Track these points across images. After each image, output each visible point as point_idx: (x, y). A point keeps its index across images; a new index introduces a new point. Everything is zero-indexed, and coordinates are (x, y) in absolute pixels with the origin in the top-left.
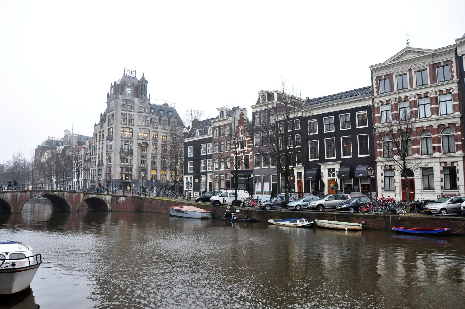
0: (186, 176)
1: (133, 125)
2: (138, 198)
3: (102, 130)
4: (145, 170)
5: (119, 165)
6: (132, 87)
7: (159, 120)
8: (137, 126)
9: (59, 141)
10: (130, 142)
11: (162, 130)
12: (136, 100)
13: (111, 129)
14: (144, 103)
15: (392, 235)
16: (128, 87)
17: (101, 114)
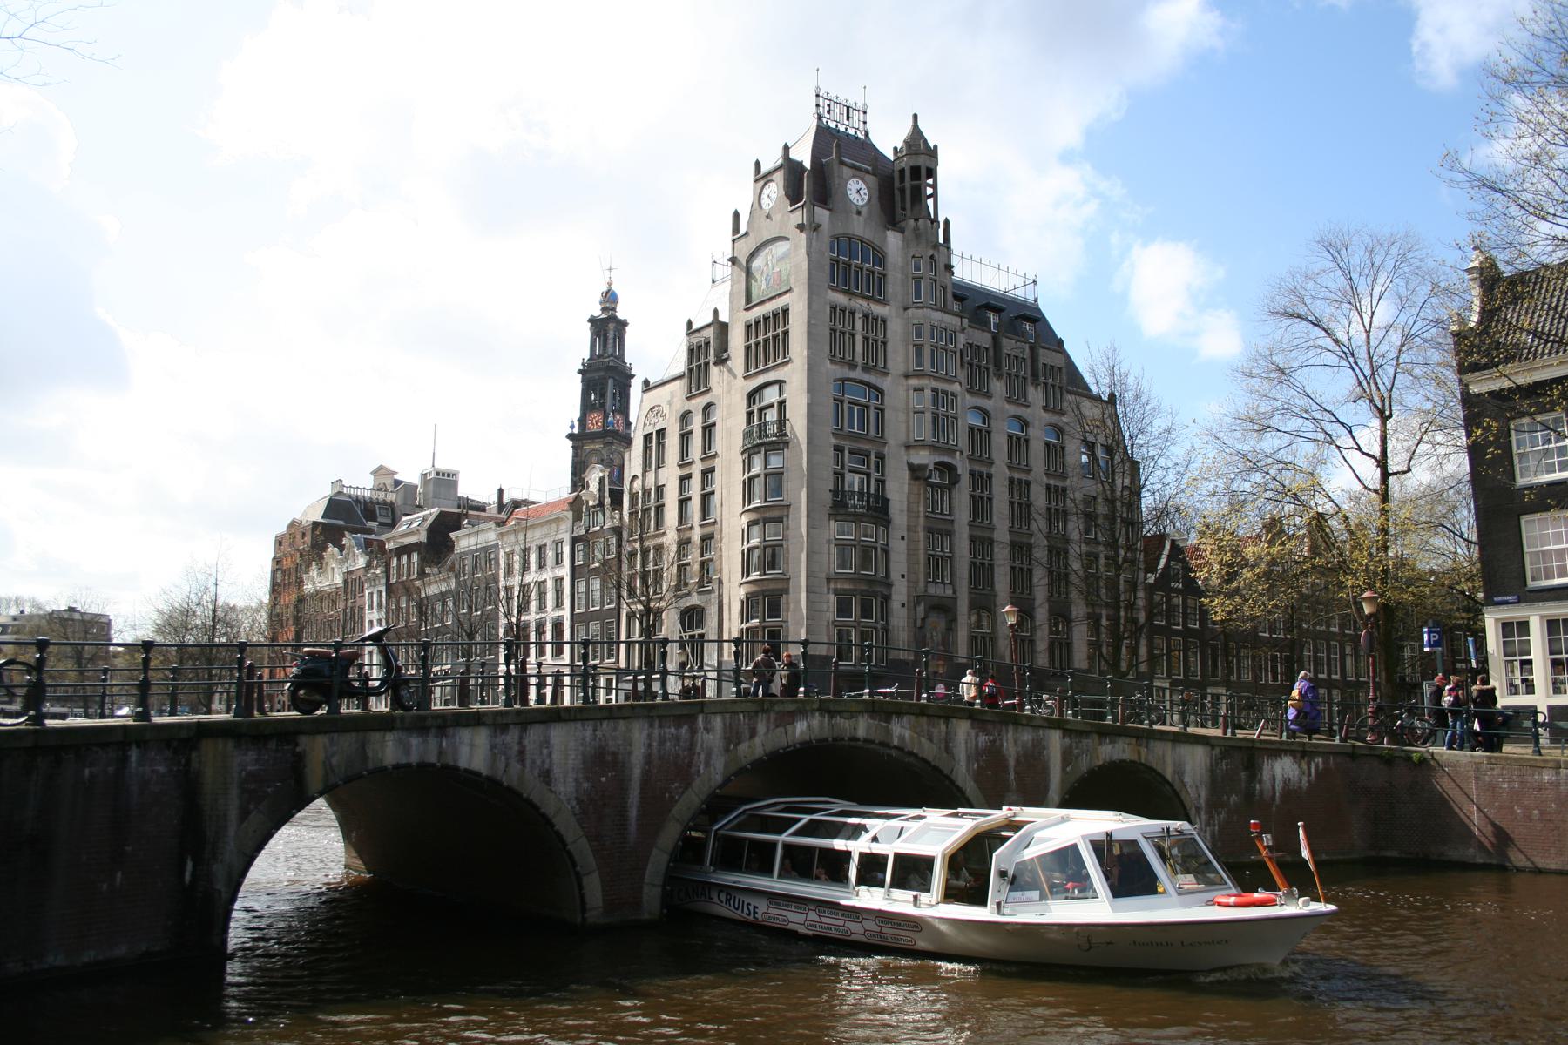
0: (1513, 613)
2: (1389, 760)
3: (701, 402)
4: (944, 608)
5: (829, 580)
6: (872, 177)
7: (991, 353)
8: (903, 380)
9: (378, 503)
10: (873, 457)
11: (1007, 406)
12: (893, 240)
13: (771, 395)
14: (932, 257)
16: (858, 173)
17: (758, 165)
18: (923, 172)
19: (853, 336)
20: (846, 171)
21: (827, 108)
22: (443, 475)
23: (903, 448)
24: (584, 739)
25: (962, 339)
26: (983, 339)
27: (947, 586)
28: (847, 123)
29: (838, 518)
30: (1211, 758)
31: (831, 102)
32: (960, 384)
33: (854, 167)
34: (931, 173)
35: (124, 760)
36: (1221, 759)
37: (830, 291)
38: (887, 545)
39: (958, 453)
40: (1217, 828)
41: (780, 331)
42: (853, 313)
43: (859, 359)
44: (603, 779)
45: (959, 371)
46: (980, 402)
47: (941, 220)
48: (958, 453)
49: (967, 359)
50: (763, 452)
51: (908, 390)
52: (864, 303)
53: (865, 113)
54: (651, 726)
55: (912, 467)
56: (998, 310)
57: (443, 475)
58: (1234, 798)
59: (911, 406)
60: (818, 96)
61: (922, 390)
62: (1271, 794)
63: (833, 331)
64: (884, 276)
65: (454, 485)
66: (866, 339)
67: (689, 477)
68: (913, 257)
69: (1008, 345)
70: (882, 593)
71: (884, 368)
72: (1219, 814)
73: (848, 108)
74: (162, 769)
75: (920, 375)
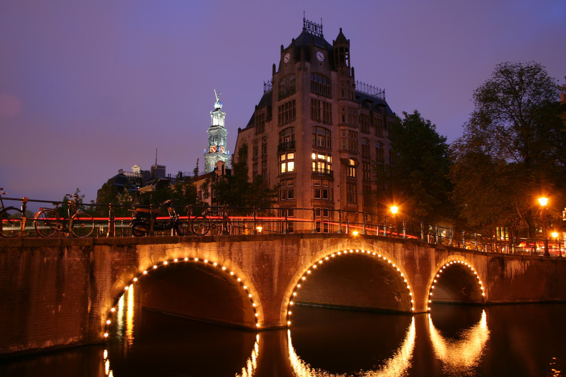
1: (331, 124)
5: (311, 202)
11: (375, 137)
12: (334, 75)
14: (348, 81)
15: (169, 208)
17: (282, 47)
18: (344, 50)
19: (319, 110)
20: (316, 49)
21: (308, 26)
22: (160, 167)
23: (338, 153)
24: (255, 249)
25: (359, 112)
26: (367, 112)
27: (355, 204)
28: (315, 32)
29: (315, 178)
30: (487, 261)
31: (310, 24)
32: (359, 128)
33: (319, 47)
34: (348, 50)
35: (62, 254)
36: (491, 262)
37: (311, 93)
38: (333, 188)
39: (358, 154)
40: (490, 289)
41: (292, 108)
42: (319, 101)
43: (322, 119)
44: (263, 266)
45: (358, 123)
46: (366, 135)
47: (351, 67)
48: (358, 154)
49: (361, 120)
50: (286, 154)
51: (339, 131)
52: (323, 98)
53: (322, 28)
54: (282, 244)
55: (341, 159)
56: (371, 102)
57: (160, 167)
58: (496, 277)
59: (341, 137)
60: (304, 21)
61: (345, 130)
62: (510, 275)
63: (312, 108)
64: (330, 88)
65: (164, 171)
66: (324, 111)
67: (257, 164)
68: (341, 81)
69: (376, 115)
70: (331, 206)
71: (331, 122)
72: (491, 283)
73: (316, 26)
74: (78, 259)
75: (344, 125)
